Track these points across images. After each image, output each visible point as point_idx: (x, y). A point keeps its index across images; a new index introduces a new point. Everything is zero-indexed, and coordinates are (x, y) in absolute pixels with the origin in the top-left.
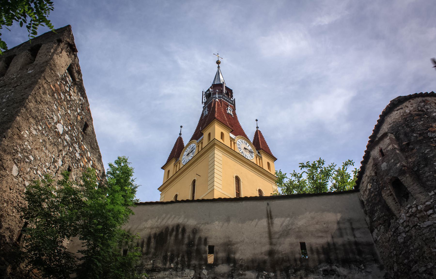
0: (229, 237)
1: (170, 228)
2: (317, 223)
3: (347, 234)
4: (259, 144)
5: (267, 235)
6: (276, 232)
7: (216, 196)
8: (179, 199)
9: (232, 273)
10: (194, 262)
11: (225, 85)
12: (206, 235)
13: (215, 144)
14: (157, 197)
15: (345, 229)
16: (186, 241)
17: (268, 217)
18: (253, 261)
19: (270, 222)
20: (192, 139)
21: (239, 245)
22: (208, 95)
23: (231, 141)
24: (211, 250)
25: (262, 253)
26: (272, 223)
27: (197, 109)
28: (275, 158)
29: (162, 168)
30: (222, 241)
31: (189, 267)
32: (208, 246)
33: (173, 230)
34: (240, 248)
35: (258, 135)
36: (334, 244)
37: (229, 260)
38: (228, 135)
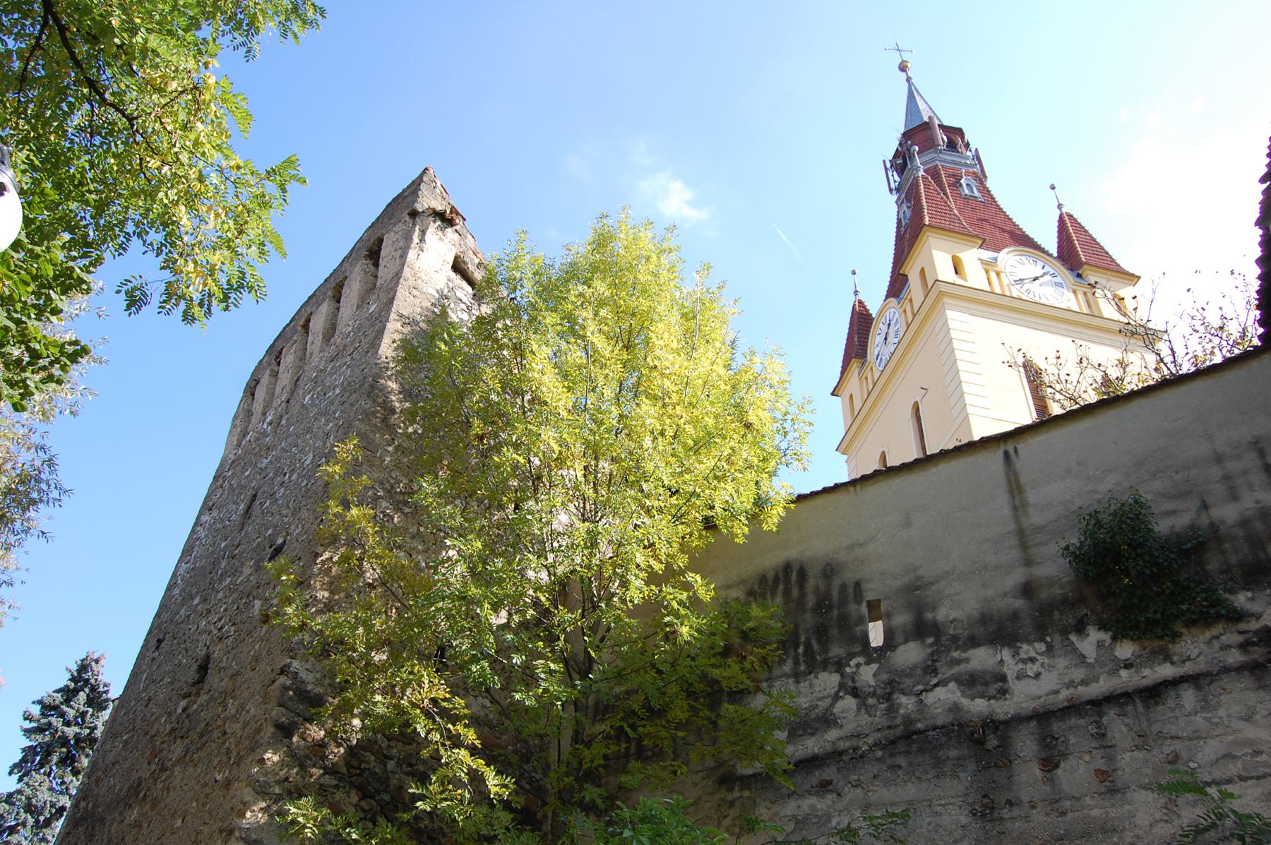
0: (915, 569)
1: (771, 575)
2: (1154, 476)
3: (1251, 488)
4: (1076, 253)
5: (1014, 541)
6: (1038, 528)
7: (976, 438)
8: (893, 462)
9: (934, 661)
10: (837, 651)
11: (937, 122)
12: (858, 576)
13: (941, 294)
14: (838, 471)
15: (1245, 473)
16: (811, 600)
17: (1019, 486)
18: (984, 619)
19: (1017, 502)
20: (887, 297)
21: (942, 584)
22: (901, 162)
23: (987, 272)
24: (875, 611)
25: (1005, 595)
26: (1024, 505)
27: (882, 213)
28: (1133, 275)
29: (833, 394)
30: (897, 583)
31: (825, 666)
32: (864, 604)
33: (776, 579)
34: (946, 592)
35: (1067, 228)
36: (1214, 527)
37: (922, 629)
38: (973, 257)
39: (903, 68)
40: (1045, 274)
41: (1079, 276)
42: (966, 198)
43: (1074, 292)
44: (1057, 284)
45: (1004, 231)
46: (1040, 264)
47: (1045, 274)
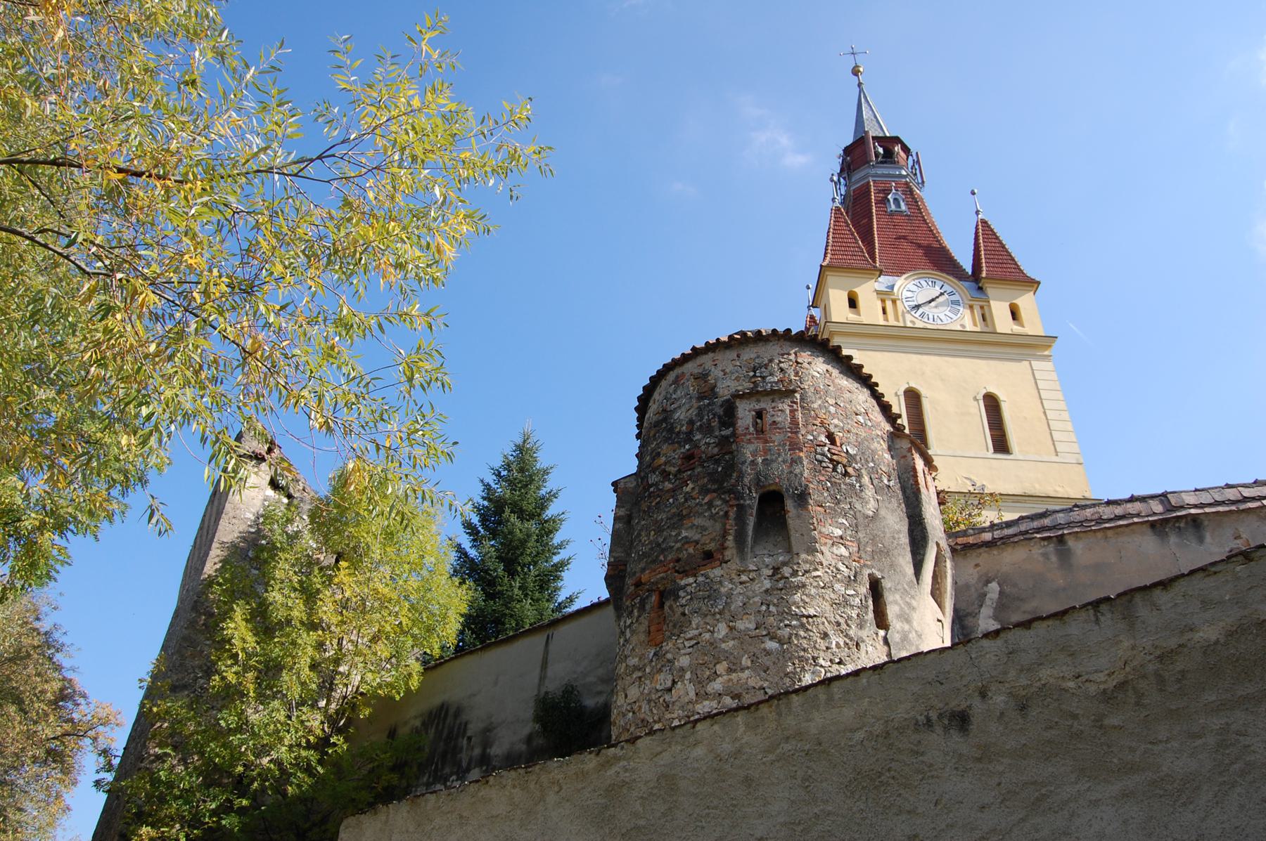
23: (883, 301)
35: (985, 234)
39: (856, 72)
40: (942, 294)
41: (980, 289)
42: (892, 214)
43: (971, 307)
44: (954, 302)
45: (919, 246)
46: (939, 283)
47: (942, 294)
